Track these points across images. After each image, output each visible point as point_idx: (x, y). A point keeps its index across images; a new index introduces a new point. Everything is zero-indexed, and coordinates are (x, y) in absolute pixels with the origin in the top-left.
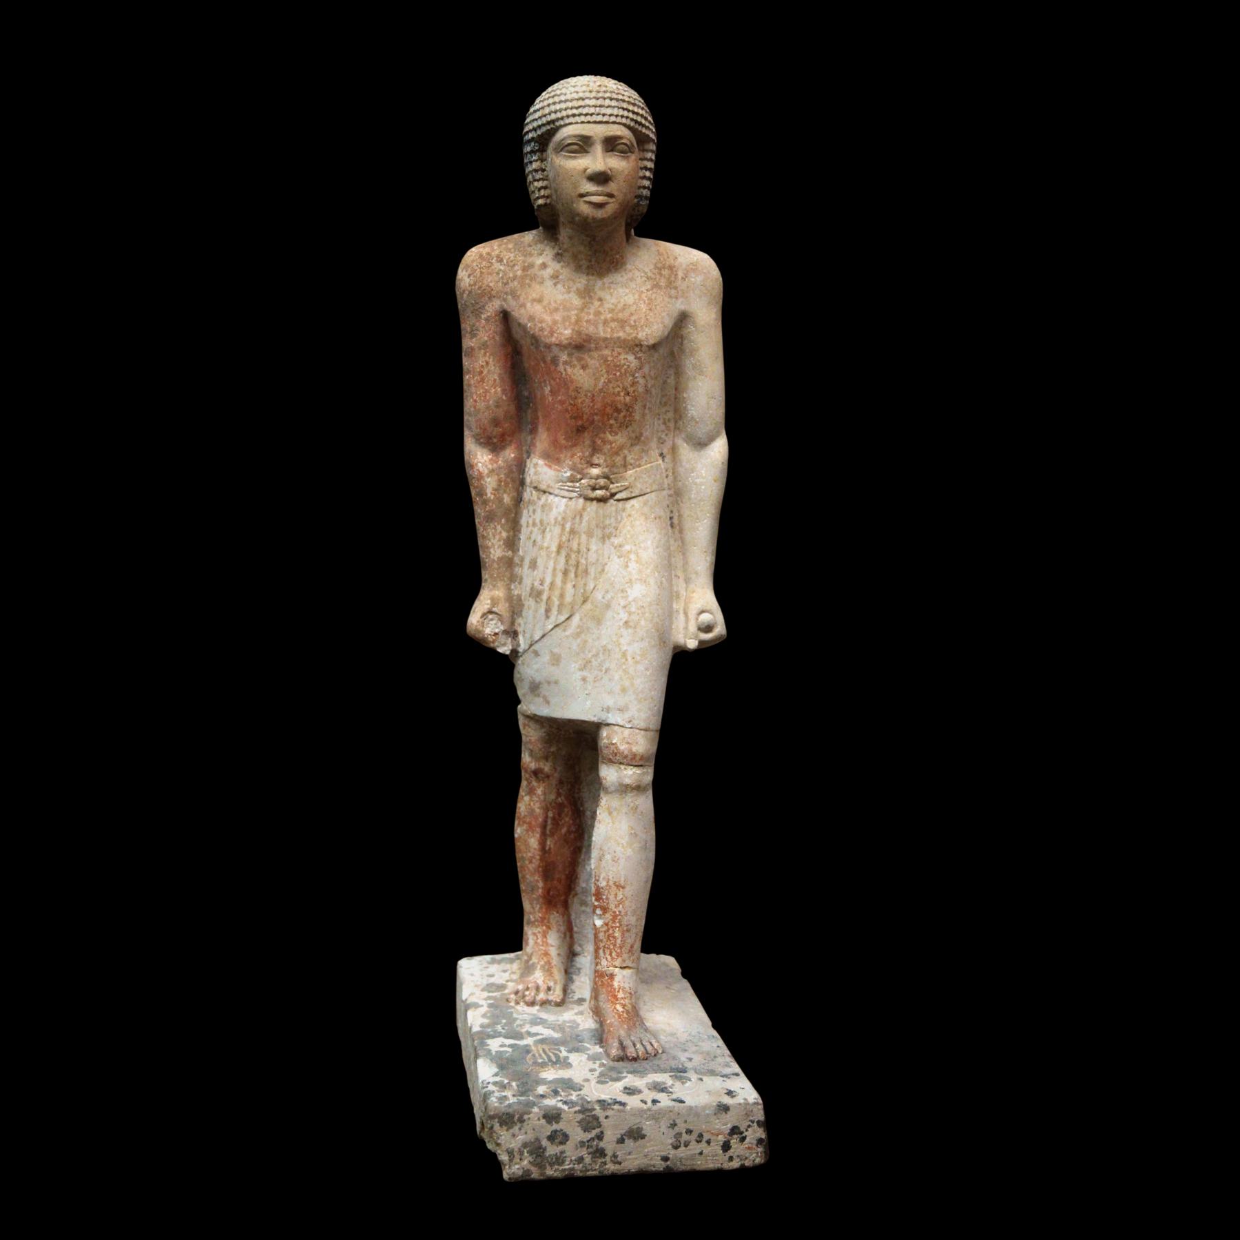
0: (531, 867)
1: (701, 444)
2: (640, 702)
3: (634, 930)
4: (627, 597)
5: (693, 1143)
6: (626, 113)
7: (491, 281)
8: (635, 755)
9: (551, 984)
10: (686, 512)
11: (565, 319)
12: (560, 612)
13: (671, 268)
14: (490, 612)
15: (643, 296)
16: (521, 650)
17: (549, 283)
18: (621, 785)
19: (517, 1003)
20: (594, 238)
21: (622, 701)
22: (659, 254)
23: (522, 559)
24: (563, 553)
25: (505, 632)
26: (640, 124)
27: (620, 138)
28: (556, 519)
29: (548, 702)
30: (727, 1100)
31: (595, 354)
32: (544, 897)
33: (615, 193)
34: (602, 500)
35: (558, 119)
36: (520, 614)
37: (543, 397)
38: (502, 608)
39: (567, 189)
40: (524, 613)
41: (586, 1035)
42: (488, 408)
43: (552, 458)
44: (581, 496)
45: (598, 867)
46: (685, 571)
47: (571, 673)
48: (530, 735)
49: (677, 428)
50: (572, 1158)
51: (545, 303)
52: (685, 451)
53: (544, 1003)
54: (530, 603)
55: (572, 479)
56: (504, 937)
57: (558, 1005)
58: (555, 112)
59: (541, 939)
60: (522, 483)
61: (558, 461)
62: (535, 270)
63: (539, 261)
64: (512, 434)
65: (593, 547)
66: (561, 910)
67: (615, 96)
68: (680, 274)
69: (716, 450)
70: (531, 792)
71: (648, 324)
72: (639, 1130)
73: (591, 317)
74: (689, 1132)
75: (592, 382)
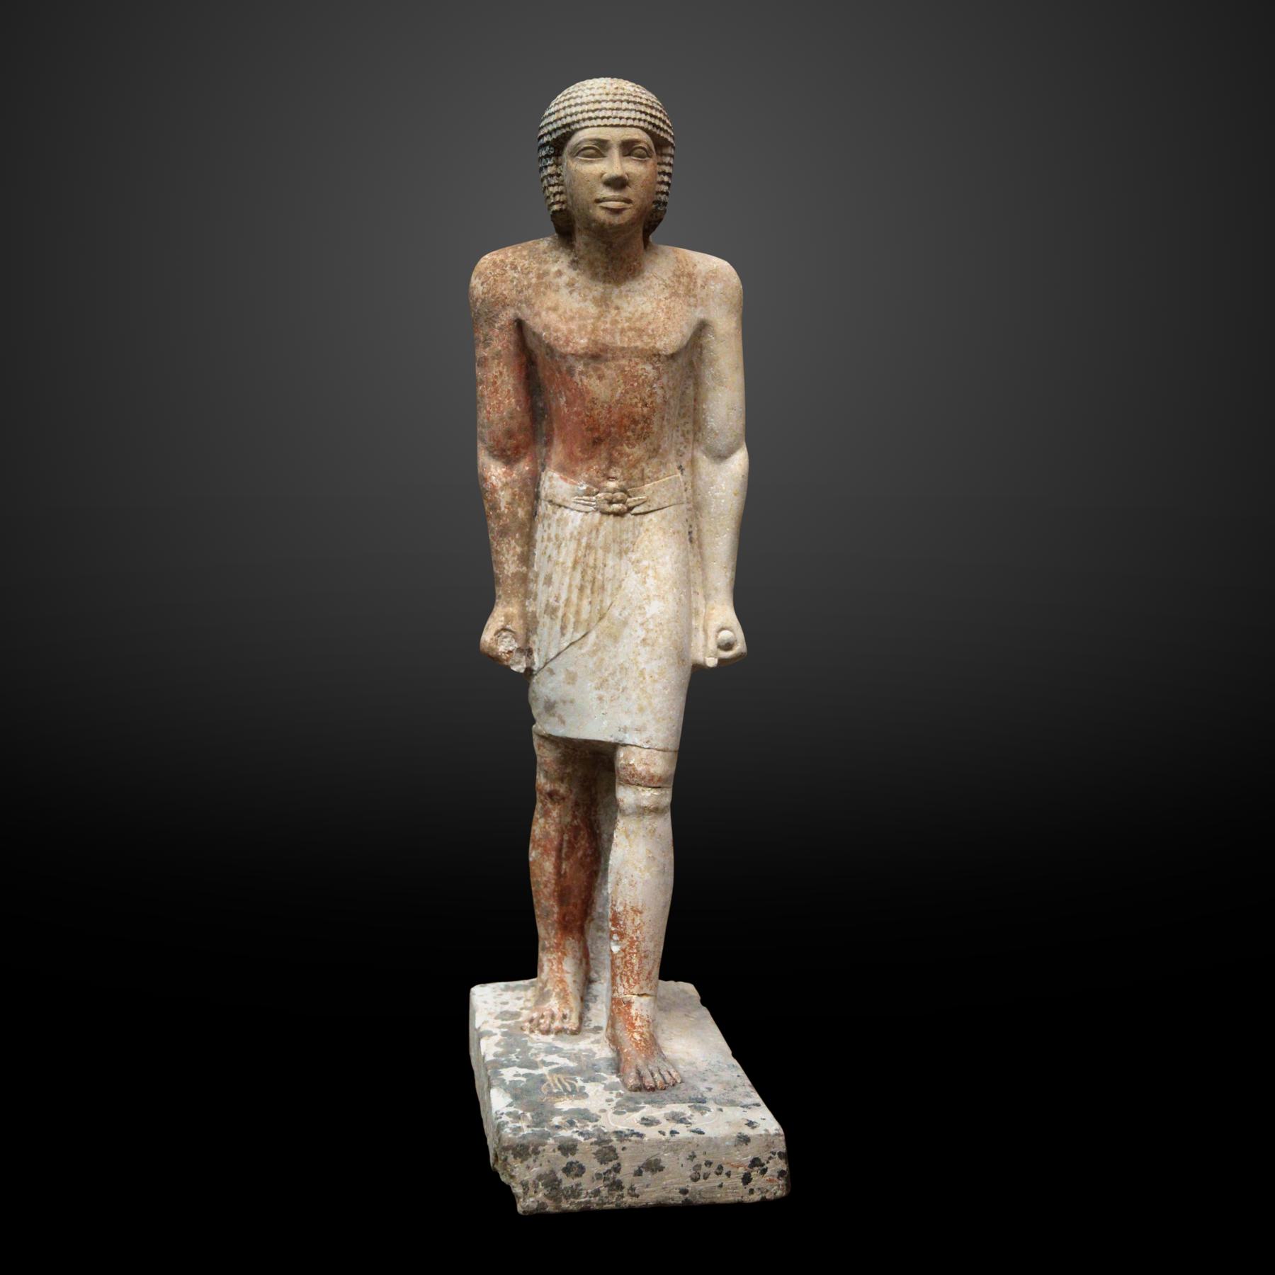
0: (546, 891)
1: (721, 457)
2: (658, 721)
3: (652, 957)
4: (645, 614)
5: (713, 1175)
6: (643, 116)
7: (504, 289)
8: (652, 777)
9: (567, 1012)
10: (705, 527)
11: (581, 328)
12: (575, 629)
13: (690, 275)
14: (504, 629)
15: (662, 304)
16: (535, 668)
17: (564, 291)
18: (639, 807)
19: (532, 1031)
20: (610, 245)
21: (639, 720)
22: (678, 261)
23: (537, 575)
24: (579, 569)
25: (520, 650)
26: (658, 127)
27: (637, 141)
28: (572, 534)
29: (563, 722)
30: (747, 1131)
31: (612, 364)
32: (560, 922)
33: (633, 199)
34: (619, 514)
35: (573, 123)
36: (534, 631)
37: (558, 408)
38: (516, 625)
39: (583, 194)
40: (539, 631)
41: (603, 1065)
42: (502, 419)
43: (567, 471)
44: (597, 510)
45: (614, 892)
46: (704, 587)
47: (587, 692)
48: (546, 756)
49: (696, 440)
50: (589, 1191)
51: (561, 311)
52: (704, 464)
53: (559, 1031)
54: (545, 620)
55: (588, 493)
56: (518, 963)
57: (574, 1033)
58: (571, 115)
59: (556, 966)
60: (537, 497)
61: (574, 474)
62: (550, 278)
63: (554, 269)
64: (527, 446)
65: (610, 563)
66: (577, 935)
67: (632, 99)
68: (700, 282)
69: (736, 462)
70: (546, 814)
71: (666, 333)
72: (657, 1162)
73: (608, 326)
74: (709, 1164)
75: (609, 393)
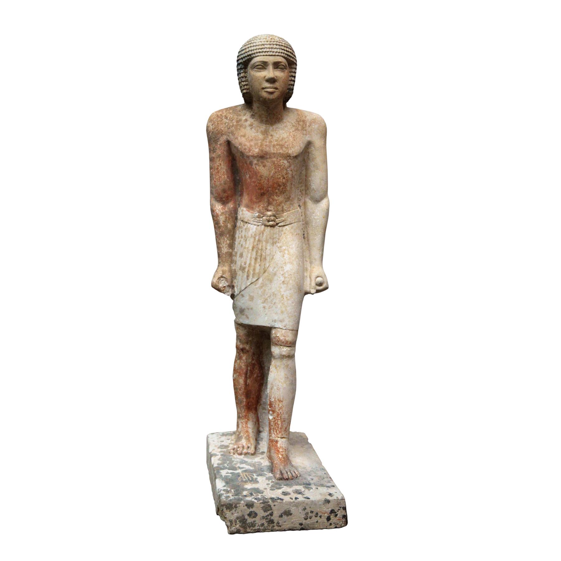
2: (289, 317)
4: (284, 270)
5: (314, 517)
6: (283, 51)
7: (222, 127)
8: (287, 342)
9: (249, 445)
10: (310, 232)
11: (256, 144)
12: (253, 277)
13: (304, 121)
14: (222, 277)
15: (291, 134)
16: (235, 294)
17: (248, 128)
18: (281, 355)
19: (234, 454)
20: (269, 108)
21: (281, 317)
22: (298, 115)
23: (236, 253)
24: (255, 250)
25: (229, 286)
26: (290, 56)
27: (280, 62)
28: (251, 235)
29: (248, 318)
30: (329, 498)
31: (269, 160)
32: (246, 406)
33: (278, 87)
34: (272, 226)
35: (252, 54)
36: (235, 278)
37: (246, 180)
38: (227, 275)
39: (257, 85)
40: (237, 278)
41: (265, 468)
42: (221, 184)
43: (250, 207)
44: (263, 224)
45: (270, 392)
46: (310, 258)
47: (258, 305)
49: (306, 194)
51: (247, 137)
52: (310, 204)
53: (246, 454)
54: (240, 273)
55: (259, 217)
57: (253, 454)
58: (251, 51)
60: (236, 218)
61: (252, 209)
62: (242, 122)
63: (244, 118)
64: (232, 196)
65: (268, 248)
66: (254, 412)
67: (278, 43)
68: (308, 124)
69: (324, 203)
71: (293, 146)
72: (289, 511)
73: (267, 143)
74: (312, 512)
75: (268, 173)
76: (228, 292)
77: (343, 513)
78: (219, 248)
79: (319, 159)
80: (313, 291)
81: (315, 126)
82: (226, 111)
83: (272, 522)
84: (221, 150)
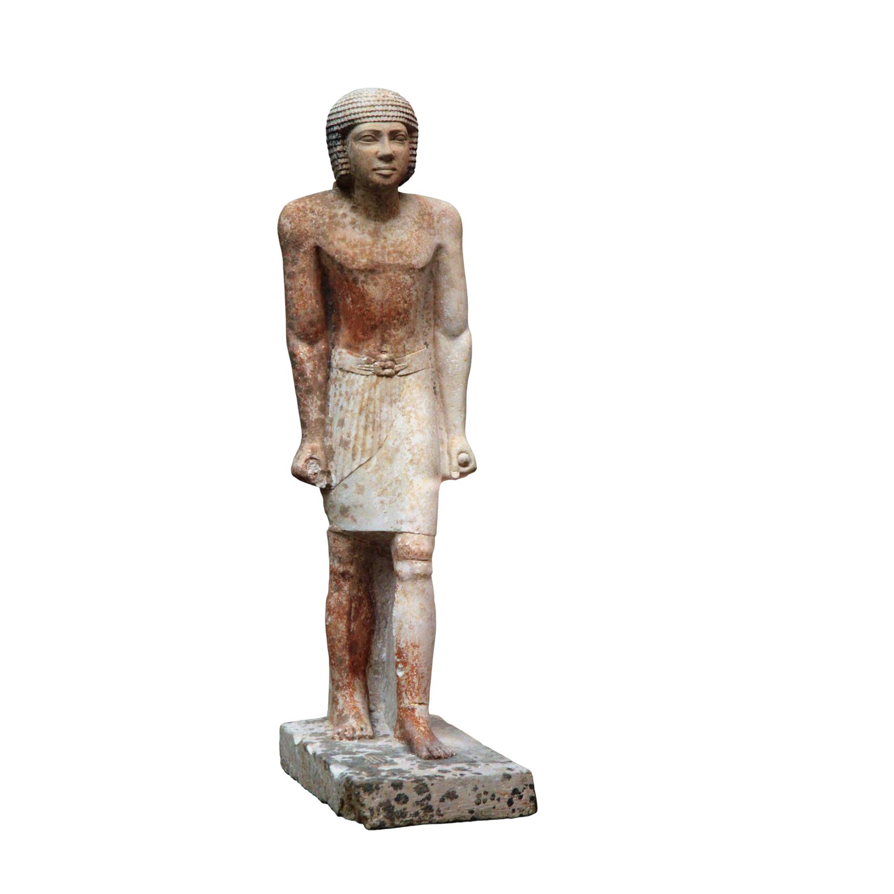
2: (424, 515)
6: (402, 115)
7: (306, 226)
8: (422, 554)
9: (363, 726)
10: (445, 383)
11: (363, 252)
12: (362, 456)
13: (429, 214)
14: (311, 458)
16: (333, 484)
17: (349, 227)
18: (414, 574)
19: (341, 739)
20: (380, 196)
21: (410, 514)
22: (421, 205)
23: (331, 420)
24: (364, 414)
25: (323, 472)
27: (399, 131)
28: (357, 390)
29: (355, 521)
30: (508, 772)
31: (383, 276)
32: (350, 668)
34: (389, 376)
35: (356, 119)
36: (332, 458)
37: (345, 305)
38: (319, 455)
39: (364, 165)
40: (335, 458)
41: (400, 750)
42: (306, 314)
43: (353, 347)
44: (374, 374)
45: (398, 634)
46: (446, 424)
47: (372, 498)
49: (436, 325)
51: (348, 241)
52: (443, 341)
53: (360, 738)
54: (339, 450)
60: (329, 366)
61: (357, 350)
62: (338, 218)
63: (341, 212)
64: (322, 332)
65: (385, 410)
66: (361, 677)
68: (436, 219)
69: (465, 339)
72: (454, 792)
74: (486, 793)
76: (321, 481)
77: (531, 794)
78: (302, 412)
79: (454, 272)
80: (456, 474)
81: (446, 221)
82: (311, 201)
83: (429, 809)
84: (305, 262)
